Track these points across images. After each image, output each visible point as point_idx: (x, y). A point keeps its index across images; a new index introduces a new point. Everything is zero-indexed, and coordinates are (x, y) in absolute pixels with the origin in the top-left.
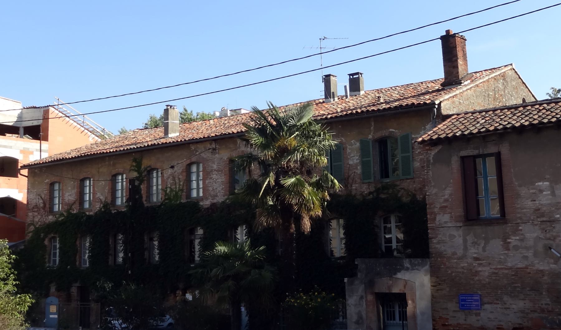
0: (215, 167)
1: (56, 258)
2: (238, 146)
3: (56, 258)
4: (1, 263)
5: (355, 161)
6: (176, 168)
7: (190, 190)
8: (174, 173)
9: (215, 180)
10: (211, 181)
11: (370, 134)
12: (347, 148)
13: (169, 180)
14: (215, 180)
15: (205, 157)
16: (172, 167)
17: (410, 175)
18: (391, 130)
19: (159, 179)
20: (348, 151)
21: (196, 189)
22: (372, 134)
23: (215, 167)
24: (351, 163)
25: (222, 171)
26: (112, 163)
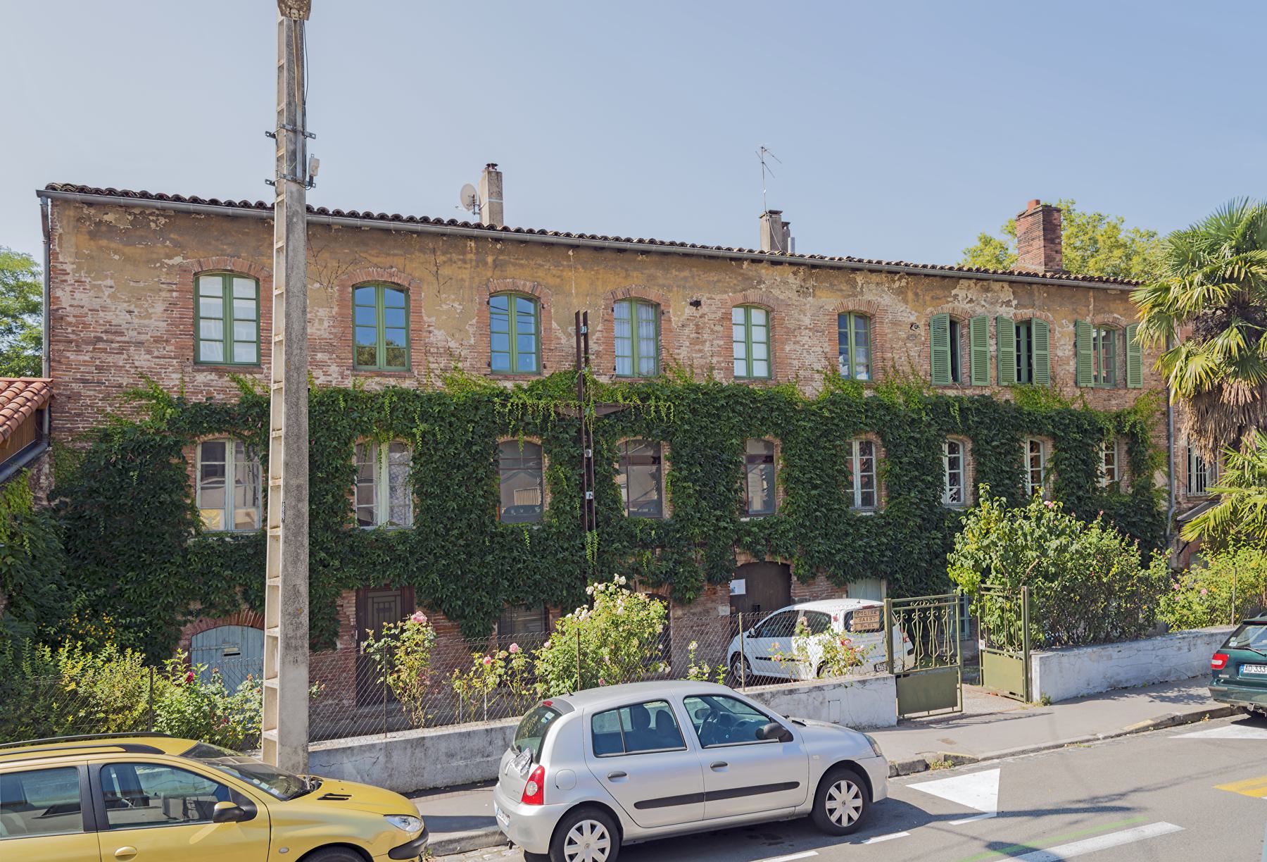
0: (807, 321)
1: (223, 463)
2: (858, 289)
3: (223, 463)
4: (11, 302)
5: (1067, 352)
6: (704, 309)
7: (730, 360)
8: (701, 317)
9: (806, 347)
10: (797, 347)
11: (1088, 315)
12: (1055, 330)
13: (687, 331)
14: (806, 347)
15: (781, 297)
16: (697, 304)
17: (585, 314)
18: (1115, 315)
19: (743, 335)
20: (1057, 335)
21: (754, 358)
22: (1091, 315)
23: (807, 321)
24: (1060, 353)
25: (823, 331)
26: (490, 259)
